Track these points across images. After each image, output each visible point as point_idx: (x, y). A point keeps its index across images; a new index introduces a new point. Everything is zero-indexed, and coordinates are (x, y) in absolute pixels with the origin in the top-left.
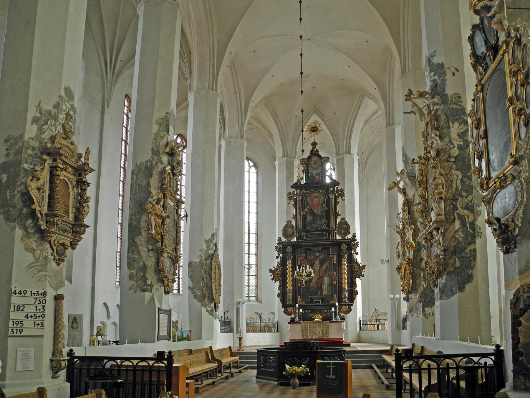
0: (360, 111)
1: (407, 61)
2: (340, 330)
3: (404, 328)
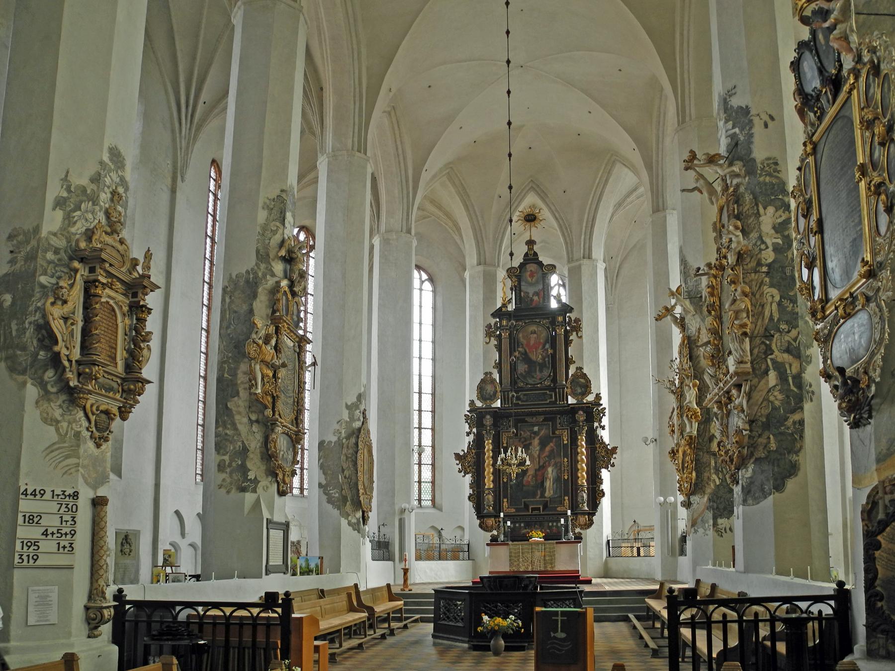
0: (608, 187)
1: (687, 102)
2: (573, 556)
3: (683, 552)
